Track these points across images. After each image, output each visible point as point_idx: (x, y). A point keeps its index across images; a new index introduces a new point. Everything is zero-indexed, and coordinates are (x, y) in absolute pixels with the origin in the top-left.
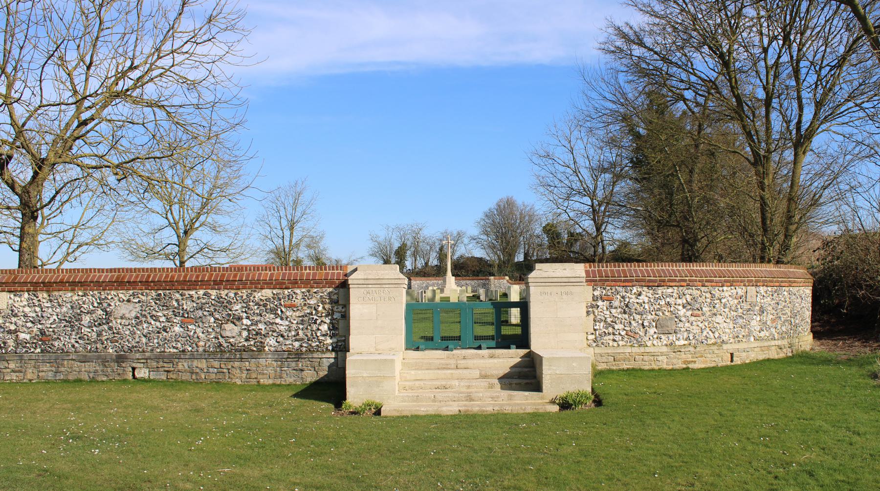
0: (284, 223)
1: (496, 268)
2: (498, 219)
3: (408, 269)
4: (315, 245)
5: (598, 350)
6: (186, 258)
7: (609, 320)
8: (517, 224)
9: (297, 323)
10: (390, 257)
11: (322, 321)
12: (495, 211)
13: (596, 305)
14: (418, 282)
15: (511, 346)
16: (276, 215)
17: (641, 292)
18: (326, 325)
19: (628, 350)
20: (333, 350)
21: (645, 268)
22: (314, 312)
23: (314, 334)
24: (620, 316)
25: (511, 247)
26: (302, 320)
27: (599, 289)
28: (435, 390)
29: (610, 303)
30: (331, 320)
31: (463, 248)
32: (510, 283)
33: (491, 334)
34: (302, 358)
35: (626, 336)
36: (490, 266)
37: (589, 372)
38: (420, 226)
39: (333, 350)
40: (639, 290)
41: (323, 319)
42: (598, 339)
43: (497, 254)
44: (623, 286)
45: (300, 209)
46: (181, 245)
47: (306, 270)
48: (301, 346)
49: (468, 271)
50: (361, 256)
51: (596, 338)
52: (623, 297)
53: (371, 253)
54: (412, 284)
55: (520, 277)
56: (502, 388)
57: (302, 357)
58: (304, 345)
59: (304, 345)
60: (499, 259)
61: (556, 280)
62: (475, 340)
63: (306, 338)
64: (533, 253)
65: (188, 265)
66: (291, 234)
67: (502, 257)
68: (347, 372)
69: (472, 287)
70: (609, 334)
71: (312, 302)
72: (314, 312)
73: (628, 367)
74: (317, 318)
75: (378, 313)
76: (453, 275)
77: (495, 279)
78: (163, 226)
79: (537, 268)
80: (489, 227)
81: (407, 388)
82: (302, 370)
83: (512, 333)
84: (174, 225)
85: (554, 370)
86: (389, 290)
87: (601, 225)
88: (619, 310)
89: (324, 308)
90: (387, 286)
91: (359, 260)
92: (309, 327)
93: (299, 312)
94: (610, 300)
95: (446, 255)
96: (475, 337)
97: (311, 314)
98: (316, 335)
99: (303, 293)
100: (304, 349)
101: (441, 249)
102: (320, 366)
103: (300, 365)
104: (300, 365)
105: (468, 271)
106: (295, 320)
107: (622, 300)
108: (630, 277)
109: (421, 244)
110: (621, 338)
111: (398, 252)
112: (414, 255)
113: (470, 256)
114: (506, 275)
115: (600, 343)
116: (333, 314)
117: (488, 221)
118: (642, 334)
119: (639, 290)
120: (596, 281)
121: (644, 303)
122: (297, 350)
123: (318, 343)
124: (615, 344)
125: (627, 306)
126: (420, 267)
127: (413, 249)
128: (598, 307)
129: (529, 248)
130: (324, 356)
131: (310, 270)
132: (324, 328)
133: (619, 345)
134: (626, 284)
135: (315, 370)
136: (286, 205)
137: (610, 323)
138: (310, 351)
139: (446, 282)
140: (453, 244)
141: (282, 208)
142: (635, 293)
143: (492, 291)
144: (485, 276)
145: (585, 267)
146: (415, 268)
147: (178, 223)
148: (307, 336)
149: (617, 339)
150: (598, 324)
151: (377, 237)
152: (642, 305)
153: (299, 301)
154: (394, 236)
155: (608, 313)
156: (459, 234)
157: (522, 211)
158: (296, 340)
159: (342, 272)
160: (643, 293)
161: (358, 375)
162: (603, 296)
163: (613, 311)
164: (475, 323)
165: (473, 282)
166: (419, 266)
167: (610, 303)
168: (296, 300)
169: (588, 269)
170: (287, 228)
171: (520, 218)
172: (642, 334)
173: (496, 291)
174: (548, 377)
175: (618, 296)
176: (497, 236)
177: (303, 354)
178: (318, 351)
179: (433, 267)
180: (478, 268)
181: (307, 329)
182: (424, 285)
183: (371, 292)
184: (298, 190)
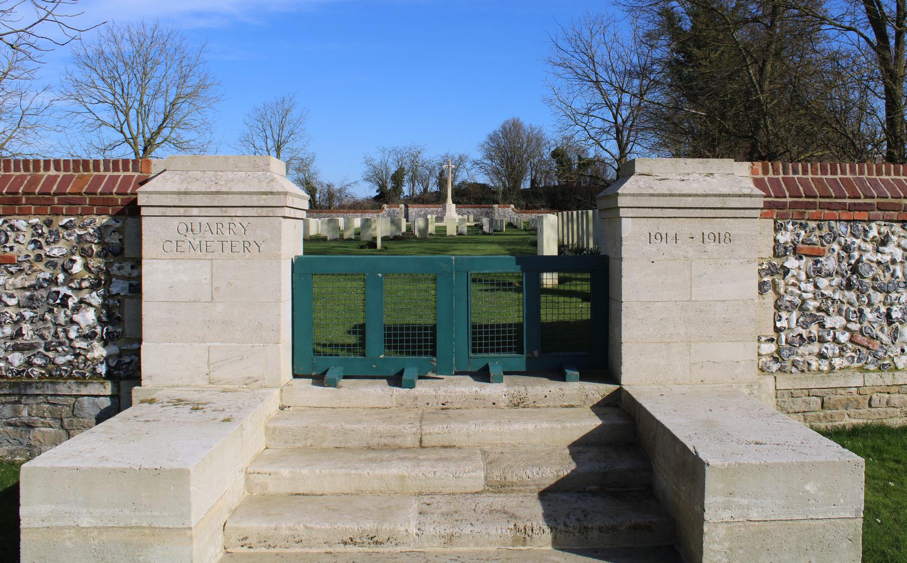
0: (271, 143)
1: (501, 196)
2: (503, 142)
3: (405, 195)
4: (305, 168)
5: (785, 382)
7: (812, 305)
8: (524, 148)
9: (18, 305)
10: (386, 183)
11: (82, 301)
12: (500, 134)
13: (783, 267)
14: (415, 209)
15: (569, 372)
16: (261, 134)
17: (887, 236)
18: (92, 310)
19: (857, 380)
20: (109, 376)
21: (893, 176)
22: (61, 277)
23: (61, 335)
24: (837, 296)
25: (517, 172)
26: (31, 298)
27: (790, 227)
28: (341, 548)
29: (816, 262)
30: (104, 297)
32: (515, 212)
33: (516, 320)
34: (28, 396)
35: (850, 345)
36: (494, 193)
37: (857, 511)
38: (419, 149)
39: (109, 376)
40: (884, 230)
41: (85, 295)
42: (785, 353)
43: (501, 180)
44: (848, 221)
45: (287, 129)
47: (47, 168)
48: (29, 363)
49: (470, 198)
50: (354, 181)
51: (778, 351)
52: (846, 248)
53: (365, 177)
54: (409, 211)
55: (527, 205)
56: (557, 544)
57: (29, 392)
58: (38, 361)
59: (38, 361)
60: (504, 185)
61: (689, 202)
62: (474, 351)
63: (43, 342)
64: (541, 179)
68: (23, 511)
69: (475, 215)
70: (811, 340)
71: (57, 251)
72: (61, 277)
73: (855, 421)
74: (69, 292)
75: (215, 285)
77: (499, 207)
78: (118, 141)
79: (638, 168)
80: (493, 151)
81: (252, 540)
82: (29, 426)
83: (555, 318)
84: (132, 141)
85: (740, 507)
86: (245, 222)
87: (627, 144)
88: (837, 280)
89: (86, 266)
90: (239, 212)
91: (353, 185)
92: (48, 316)
93: (23, 276)
94: (815, 256)
95: (446, 181)
96: (474, 327)
97: (53, 281)
98: (67, 338)
99: (34, 227)
100: (37, 371)
101: (441, 174)
102: (75, 416)
103: (25, 413)
104: (25, 413)
105: (470, 198)
106: (12, 296)
107: (844, 254)
108: (866, 197)
109: (419, 169)
110: (837, 352)
111: (395, 176)
112: (412, 180)
113: (473, 182)
114: (512, 203)
115: (788, 364)
116: (109, 282)
117: (492, 144)
118: (885, 338)
119: (884, 230)
120: (782, 206)
121: (894, 262)
122: (19, 373)
123: (70, 357)
124: (825, 366)
125: (855, 269)
126: (418, 194)
127: (410, 174)
128: (786, 271)
129: (536, 174)
130: (84, 391)
131: (57, 168)
132: (88, 317)
133: (832, 368)
134: (857, 215)
135: (62, 427)
136: (272, 124)
137: (814, 312)
138: (53, 375)
139: (445, 209)
140: (454, 169)
141: (268, 128)
142: (873, 240)
143: (496, 221)
144: (488, 204)
145: (754, 172)
146: (413, 194)
147: (137, 138)
148: (42, 337)
149: (829, 353)
150: (784, 315)
151: (372, 160)
152: (888, 268)
153: (23, 248)
154: (390, 160)
155: (810, 287)
156: (460, 158)
157: (529, 134)
158: (16, 348)
159: (136, 174)
160: (894, 238)
161: (60, 523)
162: (800, 245)
163: (823, 282)
164: (474, 281)
165: (475, 211)
166: (417, 192)
167: (816, 262)
168: (17, 247)
169: (760, 175)
170: (273, 149)
171: (528, 142)
172: (885, 338)
173: (502, 221)
174: (722, 530)
175: (836, 246)
176: (502, 161)
177: (30, 384)
178: (71, 377)
179: (432, 194)
180: (480, 195)
181: (43, 319)
182: (423, 213)
183: (196, 228)
184: (286, 107)
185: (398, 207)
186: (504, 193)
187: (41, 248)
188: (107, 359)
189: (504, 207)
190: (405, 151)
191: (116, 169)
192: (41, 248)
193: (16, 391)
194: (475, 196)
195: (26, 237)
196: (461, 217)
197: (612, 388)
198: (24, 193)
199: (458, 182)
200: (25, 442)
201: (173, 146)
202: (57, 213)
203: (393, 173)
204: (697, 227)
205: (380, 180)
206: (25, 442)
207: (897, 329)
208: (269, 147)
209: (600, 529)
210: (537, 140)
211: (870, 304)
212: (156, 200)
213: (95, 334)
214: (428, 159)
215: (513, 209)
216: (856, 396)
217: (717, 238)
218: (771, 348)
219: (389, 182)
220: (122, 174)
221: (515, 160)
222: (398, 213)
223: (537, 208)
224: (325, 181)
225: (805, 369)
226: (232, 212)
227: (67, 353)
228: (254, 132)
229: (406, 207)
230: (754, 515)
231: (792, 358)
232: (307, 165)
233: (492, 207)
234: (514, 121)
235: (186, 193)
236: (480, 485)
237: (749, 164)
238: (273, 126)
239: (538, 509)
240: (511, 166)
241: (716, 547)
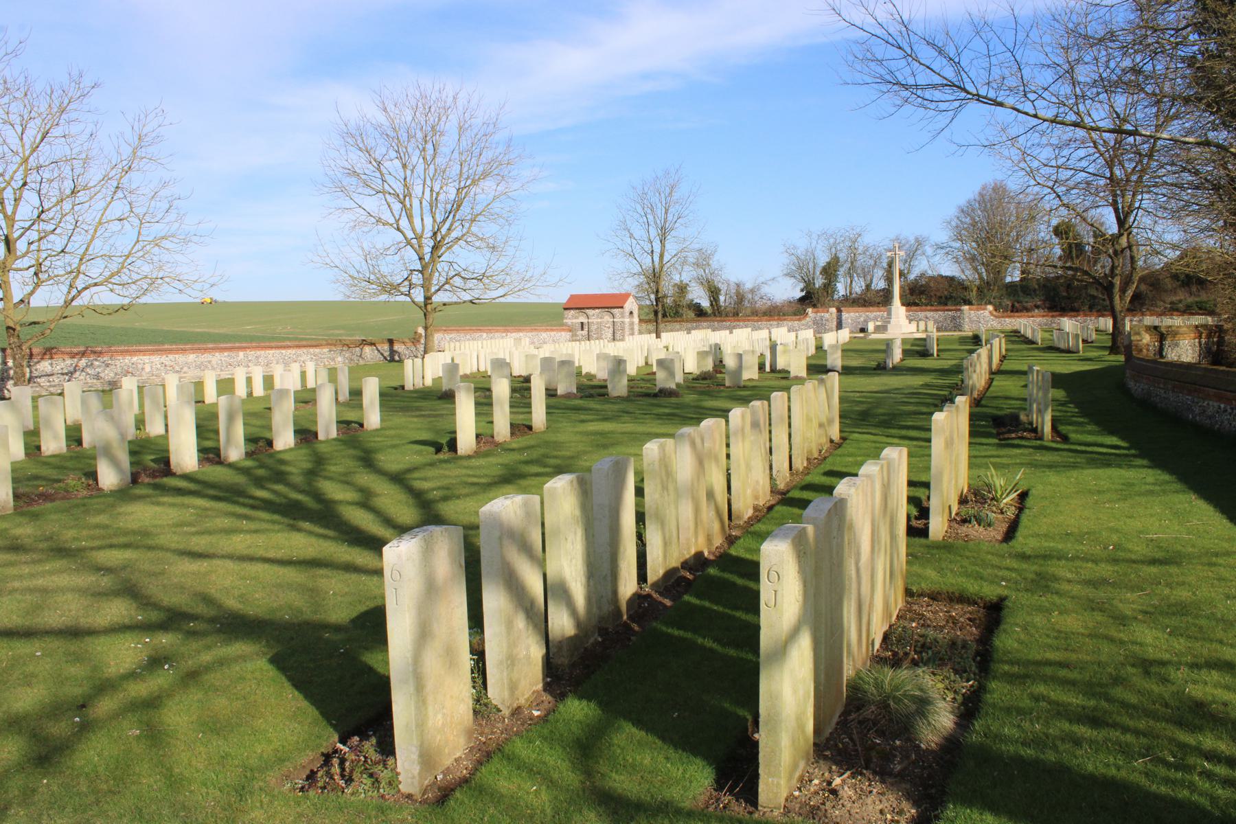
0: (653, 232)
1: (974, 293)
6: (433, 289)
14: (852, 314)
31: (925, 262)
36: (965, 288)
46: (426, 269)
49: (931, 296)
54: (843, 318)
55: (1013, 306)
60: (981, 278)
65: (435, 299)
67: (984, 274)
69: (936, 321)
76: (903, 304)
91: (770, 283)
112: (850, 274)
114: (990, 303)
127: (848, 265)
142: (297, 813)
146: (851, 293)
151: (795, 248)
156: (917, 240)
165: (937, 315)
179: (878, 291)
180: (946, 293)
185: (828, 311)
194: (938, 294)
215: (990, 312)
222: (827, 320)
223: (1027, 310)
224: (733, 279)
229: (839, 311)
233: (960, 310)
234: (995, 184)
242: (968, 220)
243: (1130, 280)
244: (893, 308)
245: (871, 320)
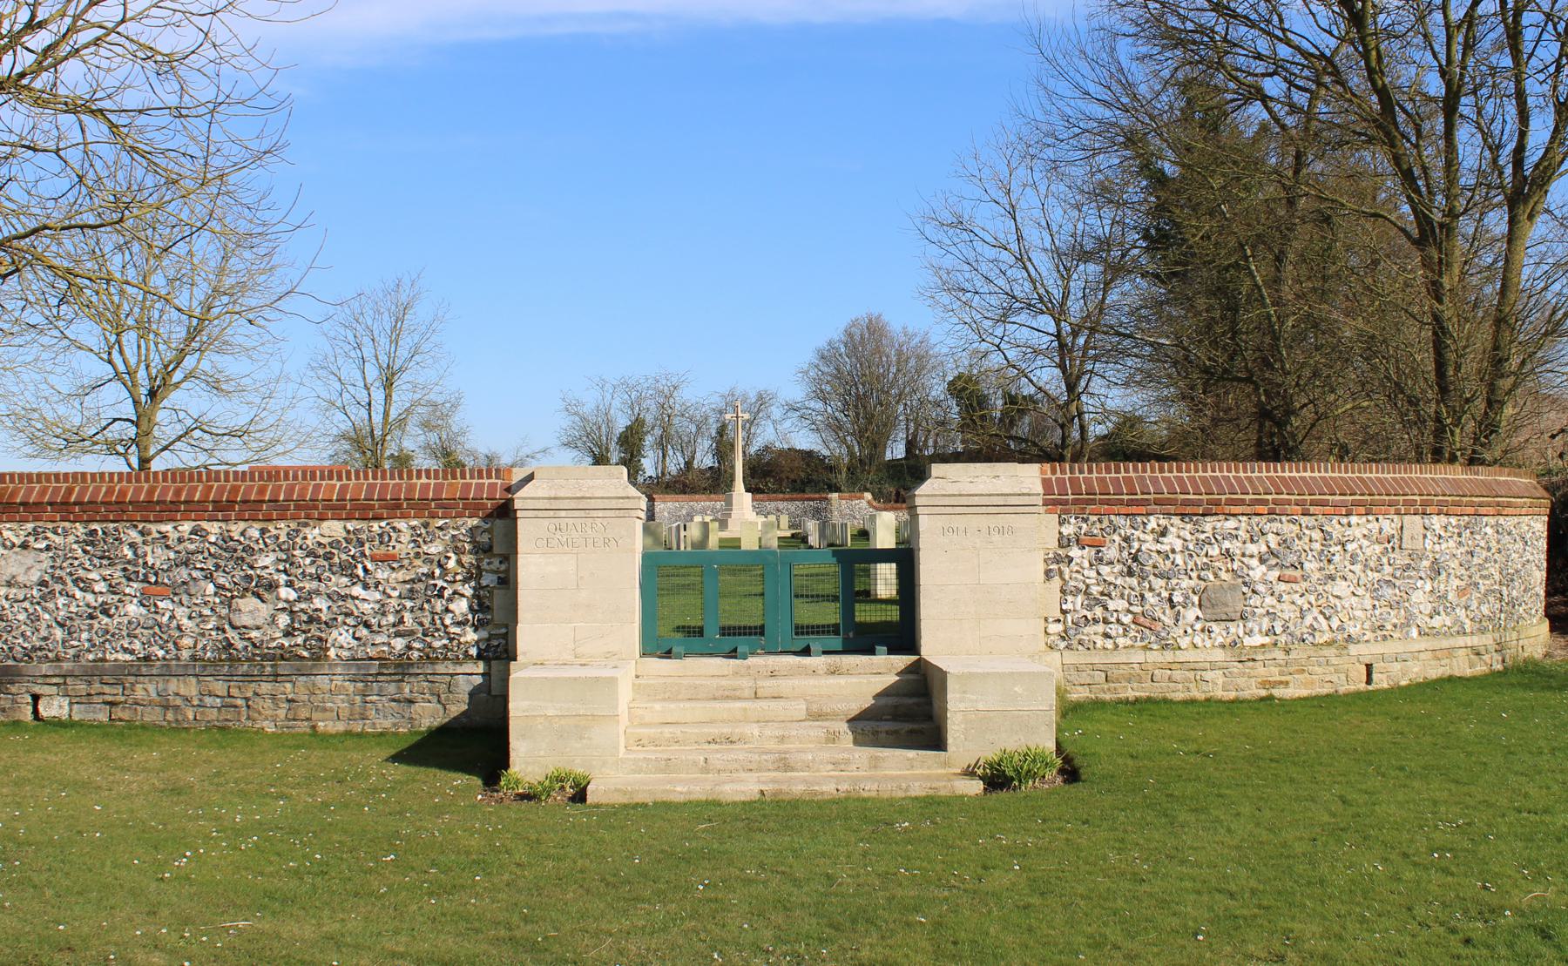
0: (372, 373)
1: (844, 475)
2: (847, 364)
3: (647, 475)
5: (1070, 658)
6: (152, 451)
7: (1095, 590)
9: (400, 597)
10: (607, 450)
11: (455, 593)
12: (842, 346)
13: (1067, 556)
15: (878, 648)
16: (353, 354)
17: (1166, 528)
18: (465, 600)
19: (1139, 657)
20: (480, 657)
21: (1175, 474)
22: (437, 572)
23: (438, 622)
24: (1119, 581)
25: (878, 426)
26: (411, 590)
27: (1073, 520)
29: (1098, 552)
30: (474, 589)
31: (770, 429)
32: (874, 508)
34: (410, 675)
35: (1133, 626)
36: (831, 469)
37: (1051, 705)
38: (674, 380)
39: (480, 657)
41: (459, 587)
42: (1072, 632)
43: (844, 441)
44: (1127, 515)
45: (406, 343)
46: (142, 420)
47: (419, 477)
48: (409, 648)
51: (1065, 631)
52: (1126, 539)
53: (565, 440)
54: (657, 510)
55: (898, 494)
56: (856, 742)
57: (411, 671)
59: (416, 645)
60: (851, 453)
61: (976, 500)
62: (797, 634)
64: (926, 440)
66: (388, 397)
67: (857, 449)
70: (1095, 621)
71: (434, 549)
72: (437, 572)
73: (1138, 694)
74: (445, 585)
80: (828, 382)
82: (411, 702)
83: (878, 619)
86: (605, 522)
87: (1079, 378)
88: (1118, 568)
89: (459, 562)
90: (600, 513)
91: (538, 456)
92: (426, 606)
94: (1098, 546)
96: (797, 627)
97: (432, 575)
98: (443, 624)
99: (413, 528)
100: (416, 654)
101: (722, 431)
103: (407, 690)
106: (394, 589)
107: (1124, 544)
108: (1143, 493)
109: (676, 421)
110: (1121, 631)
111: (626, 437)
112: (662, 445)
113: (786, 446)
114: (867, 490)
115: (1075, 642)
116: (479, 576)
117: (826, 369)
118: (1168, 620)
119: (1163, 522)
120: (1065, 503)
121: (1173, 551)
122: (400, 655)
123: (445, 641)
124: (1109, 644)
125: (1135, 559)
126: (674, 472)
127: (657, 431)
128: (1071, 560)
129: (916, 429)
130: (460, 670)
131: (428, 477)
132: (461, 607)
133: (1116, 646)
134: (1134, 509)
135: (439, 702)
136: (376, 333)
138: (429, 658)
141: (366, 341)
142: (1153, 531)
143: (834, 526)
144: (819, 492)
145: (1043, 472)
146: (663, 474)
147: (136, 372)
148: (421, 624)
149: (1113, 633)
150: (1070, 598)
151: (579, 403)
153: (403, 547)
154: (617, 403)
155: (1093, 574)
156: (760, 397)
158: (398, 635)
159: (499, 482)
162: (1082, 537)
163: (1105, 570)
164: (797, 596)
165: (792, 506)
167: (1098, 552)
168: (398, 546)
169: (1049, 475)
170: (377, 384)
173: (844, 526)
174: (959, 717)
178: (446, 658)
179: (702, 472)
180: (803, 475)
181: (422, 609)
183: (563, 526)
184: (404, 298)
186: (851, 469)
187: (419, 547)
188: (477, 642)
189: (851, 499)
190: (646, 385)
191: (481, 477)
192: (419, 547)
193: (400, 671)
194: (792, 476)
195: (405, 538)
196: (762, 519)
197: (914, 658)
198: (406, 499)
199: (756, 448)
200: (407, 715)
201: (203, 385)
202: (434, 516)
203: (621, 430)
204: (984, 522)
205: (596, 445)
206: (407, 715)
207: (1179, 612)
208: (369, 381)
209: (887, 733)
210: (918, 359)
211: (1151, 589)
212: (530, 504)
213: (468, 621)
214: (693, 401)
216: (1139, 671)
217: (1001, 531)
218: (1059, 627)
219: (615, 450)
220: (486, 481)
221: (873, 402)
224: (483, 450)
225: (1091, 647)
226: (594, 513)
227: (442, 638)
228: (338, 351)
230: (981, 707)
231: (1078, 637)
232: (443, 417)
234: (870, 320)
235: (555, 498)
236: (803, 715)
237: (1038, 465)
238: (377, 339)
239: (846, 725)
240: (866, 413)
241: (955, 727)
242: (831, 370)
243: (1081, 452)
244: (735, 495)
245: (698, 513)
